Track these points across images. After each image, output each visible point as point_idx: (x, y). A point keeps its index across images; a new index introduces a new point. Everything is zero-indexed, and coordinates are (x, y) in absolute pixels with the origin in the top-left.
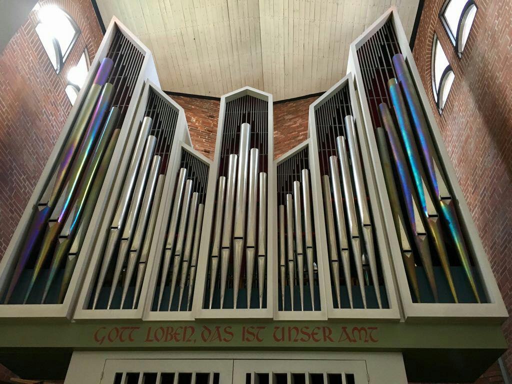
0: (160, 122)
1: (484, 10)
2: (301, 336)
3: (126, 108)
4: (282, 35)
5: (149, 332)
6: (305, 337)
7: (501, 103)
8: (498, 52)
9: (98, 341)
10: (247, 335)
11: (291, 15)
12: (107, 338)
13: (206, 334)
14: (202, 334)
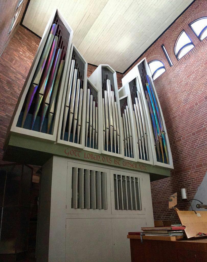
0: (77, 64)
1: (168, 73)
2: (130, 165)
3: (73, 56)
4: (93, 40)
5: (85, 155)
6: (131, 166)
7: (167, 102)
8: (171, 87)
9: (67, 154)
10: (116, 162)
11: (101, 36)
12: (70, 153)
13: (104, 159)
14: (103, 159)
